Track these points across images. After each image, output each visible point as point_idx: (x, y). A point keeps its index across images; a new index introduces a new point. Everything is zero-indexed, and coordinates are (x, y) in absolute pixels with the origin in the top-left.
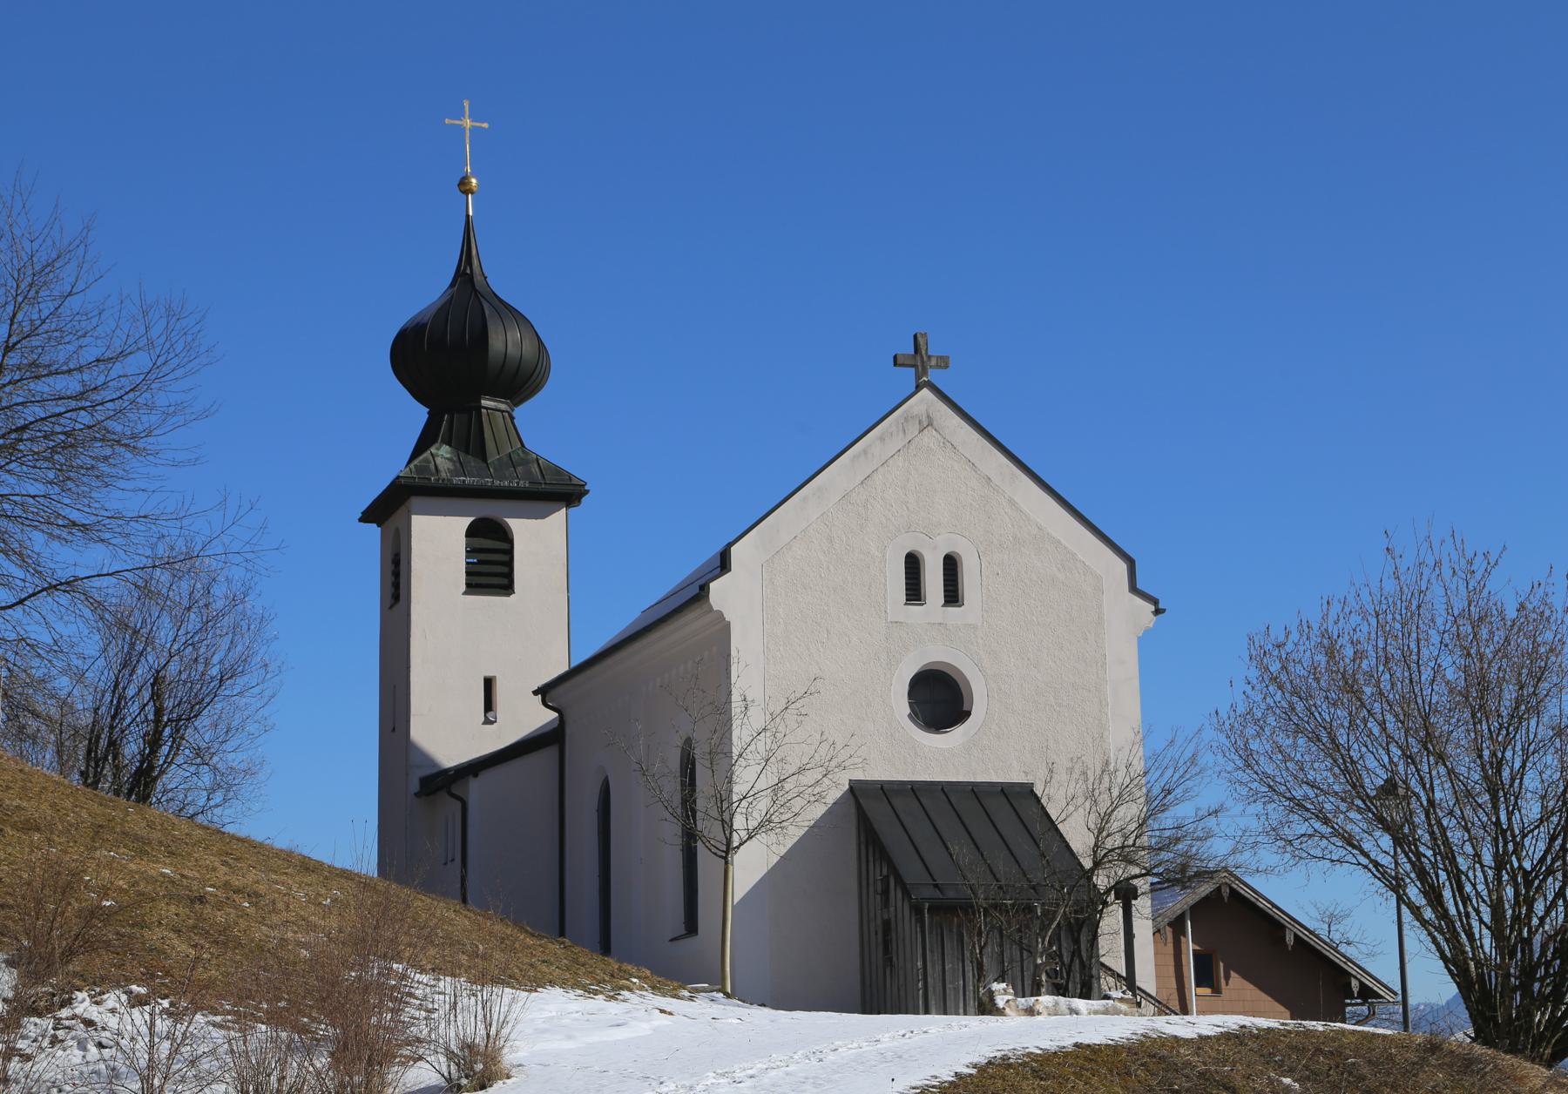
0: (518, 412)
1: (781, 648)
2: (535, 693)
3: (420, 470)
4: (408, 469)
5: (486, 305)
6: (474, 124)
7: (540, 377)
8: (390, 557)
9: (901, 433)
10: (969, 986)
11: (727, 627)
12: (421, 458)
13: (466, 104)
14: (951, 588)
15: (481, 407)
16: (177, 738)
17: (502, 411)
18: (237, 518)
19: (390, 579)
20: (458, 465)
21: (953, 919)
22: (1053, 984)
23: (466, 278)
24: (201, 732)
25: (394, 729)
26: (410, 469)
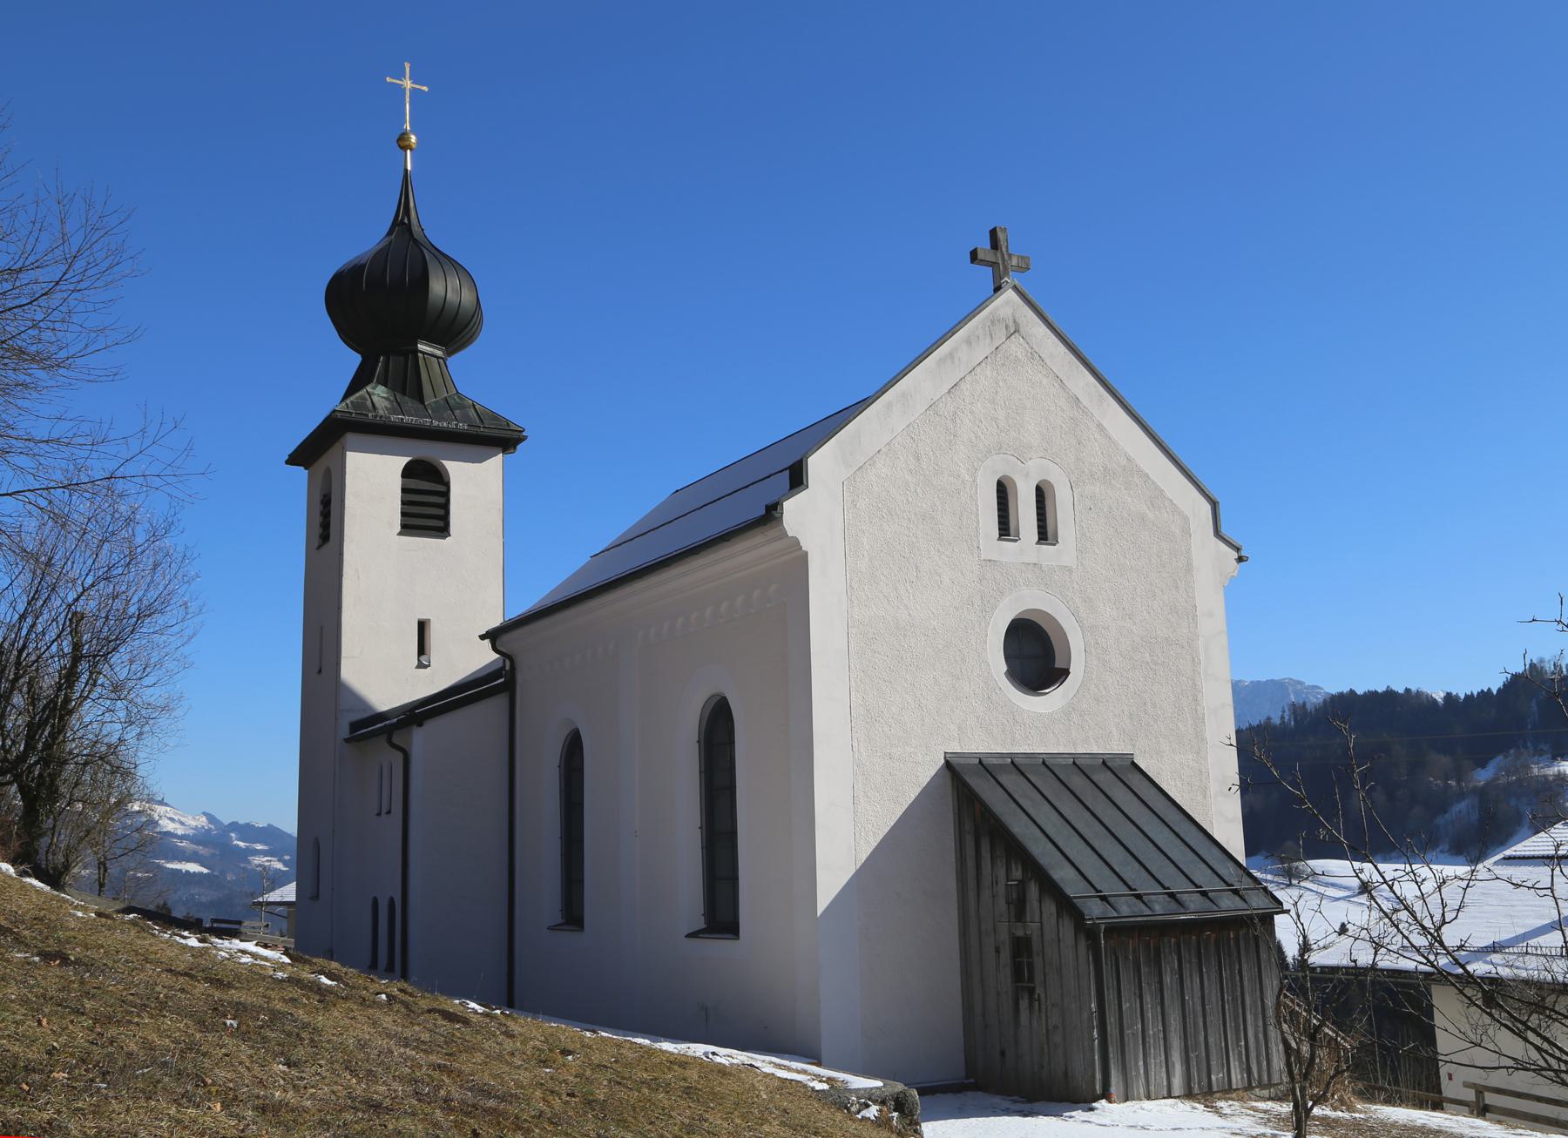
0: (452, 361)
1: (866, 588)
2: (482, 637)
3: (355, 405)
4: (344, 404)
5: (425, 251)
6: (414, 86)
7: (474, 330)
8: (318, 498)
9: (988, 337)
10: (1149, 1030)
11: (803, 559)
12: (357, 395)
14: (1004, 527)
15: (417, 351)
16: (94, 672)
17: (438, 358)
18: (158, 438)
19: (318, 519)
21: (1129, 942)
23: (402, 226)
24: (120, 665)
25: (320, 671)
26: (347, 405)
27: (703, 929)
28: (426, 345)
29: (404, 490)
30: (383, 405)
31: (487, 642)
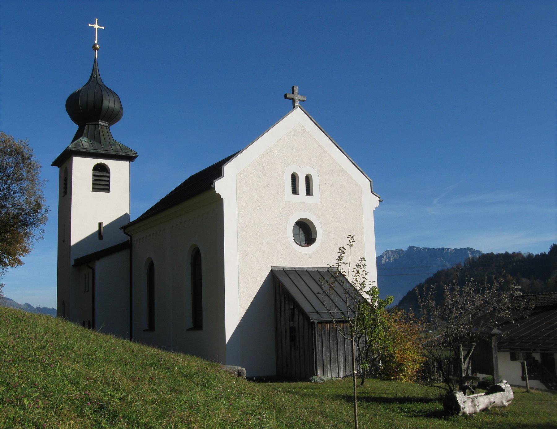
0: (112, 127)
2: (121, 229)
4: (72, 144)
12: (77, 141)
13: (97, 20)
17: (106, 127)
20: (90, 144)
22: (491, 373)
25: (64, 241)
27: (192, 328)
28: (102, 122)
29: (94, 175)
30: (86, 145)
31: (122, 230)
